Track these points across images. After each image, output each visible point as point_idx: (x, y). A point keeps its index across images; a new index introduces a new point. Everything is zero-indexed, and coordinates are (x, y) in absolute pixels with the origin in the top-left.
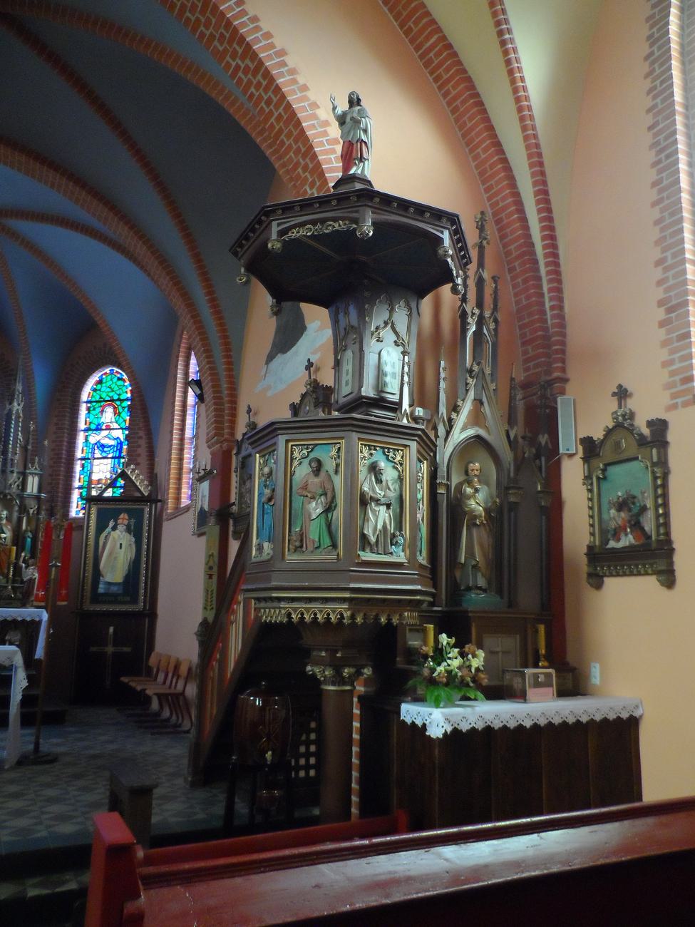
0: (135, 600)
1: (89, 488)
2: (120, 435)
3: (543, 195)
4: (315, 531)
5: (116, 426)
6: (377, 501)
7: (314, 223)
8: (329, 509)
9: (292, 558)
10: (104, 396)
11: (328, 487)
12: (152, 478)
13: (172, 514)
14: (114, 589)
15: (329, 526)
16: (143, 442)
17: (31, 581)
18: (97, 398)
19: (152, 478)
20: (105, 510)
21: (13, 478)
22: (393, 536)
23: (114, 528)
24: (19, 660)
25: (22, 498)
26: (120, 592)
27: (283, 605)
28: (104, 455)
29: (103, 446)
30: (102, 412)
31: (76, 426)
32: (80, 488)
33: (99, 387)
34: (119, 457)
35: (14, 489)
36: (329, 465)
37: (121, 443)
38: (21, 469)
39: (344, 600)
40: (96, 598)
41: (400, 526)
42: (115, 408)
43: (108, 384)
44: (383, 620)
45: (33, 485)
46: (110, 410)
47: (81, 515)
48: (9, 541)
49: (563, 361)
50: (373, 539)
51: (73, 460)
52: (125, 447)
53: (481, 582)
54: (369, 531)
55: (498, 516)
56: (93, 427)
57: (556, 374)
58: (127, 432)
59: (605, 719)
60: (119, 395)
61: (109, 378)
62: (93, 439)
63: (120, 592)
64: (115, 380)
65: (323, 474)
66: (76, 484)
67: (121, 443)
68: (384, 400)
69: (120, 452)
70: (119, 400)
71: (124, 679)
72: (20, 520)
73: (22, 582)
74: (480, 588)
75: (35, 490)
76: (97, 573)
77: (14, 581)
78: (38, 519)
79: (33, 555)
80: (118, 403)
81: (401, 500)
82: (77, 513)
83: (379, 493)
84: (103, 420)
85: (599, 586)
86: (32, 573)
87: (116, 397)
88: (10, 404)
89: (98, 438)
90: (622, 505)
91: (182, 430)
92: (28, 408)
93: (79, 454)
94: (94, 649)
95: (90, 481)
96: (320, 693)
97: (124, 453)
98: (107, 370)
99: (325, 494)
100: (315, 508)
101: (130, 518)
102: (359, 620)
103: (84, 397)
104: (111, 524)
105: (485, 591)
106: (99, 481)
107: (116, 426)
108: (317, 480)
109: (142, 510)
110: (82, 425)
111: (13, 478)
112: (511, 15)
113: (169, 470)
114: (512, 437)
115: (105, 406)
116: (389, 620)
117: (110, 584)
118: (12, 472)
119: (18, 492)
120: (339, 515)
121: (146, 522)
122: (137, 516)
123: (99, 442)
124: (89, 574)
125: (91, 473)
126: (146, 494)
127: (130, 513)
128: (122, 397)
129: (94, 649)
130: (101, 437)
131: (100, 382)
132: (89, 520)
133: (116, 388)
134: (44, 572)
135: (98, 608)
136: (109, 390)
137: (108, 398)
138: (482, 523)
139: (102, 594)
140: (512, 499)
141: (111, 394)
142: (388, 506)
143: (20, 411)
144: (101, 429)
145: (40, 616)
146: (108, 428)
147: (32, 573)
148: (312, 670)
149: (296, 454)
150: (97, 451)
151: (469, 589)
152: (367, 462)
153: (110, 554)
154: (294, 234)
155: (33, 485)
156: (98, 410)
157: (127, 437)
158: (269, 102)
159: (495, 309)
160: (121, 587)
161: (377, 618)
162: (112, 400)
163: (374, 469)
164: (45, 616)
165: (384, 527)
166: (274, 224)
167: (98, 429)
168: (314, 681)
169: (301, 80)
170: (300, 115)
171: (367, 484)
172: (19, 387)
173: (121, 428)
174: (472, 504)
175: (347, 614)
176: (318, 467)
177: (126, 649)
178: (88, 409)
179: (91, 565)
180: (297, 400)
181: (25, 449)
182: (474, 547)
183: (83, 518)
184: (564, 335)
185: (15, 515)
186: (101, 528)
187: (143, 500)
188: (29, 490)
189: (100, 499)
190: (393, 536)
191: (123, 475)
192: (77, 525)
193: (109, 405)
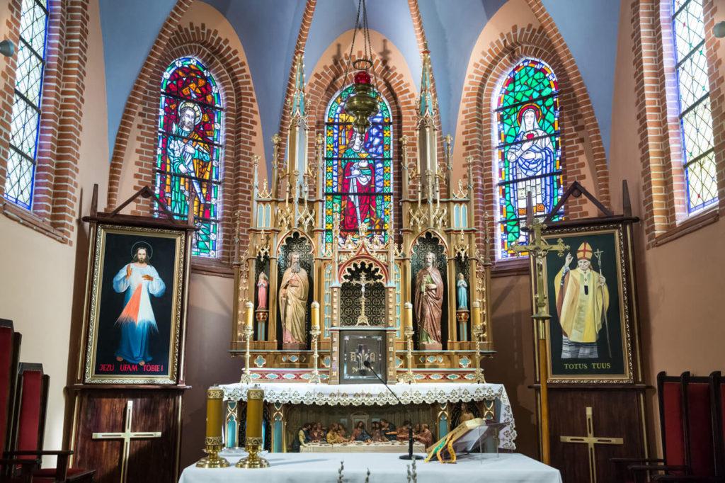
5: (541, 133)
10: (519, 97)
14: (584, 352)
23: (574, 265)
30: (520, 119)
33: (511, 87)
42: (536, 110)
43: (523, 81)
60: (540, 91)
70: (541, 98)
80: (540, 102)
87: (536, 95)
101: (594, 250)
110: (496, 141)
115: (523, 110)
117: (577, 345)
122: (604, 244)
127: (595, 242)
136: (525, 88)
137: (525, 99)
141: (528, 94)
146: (530, 137)
162: (532, 100)
173: (550, 135)
186: (555, 263)
193: (528, 108)
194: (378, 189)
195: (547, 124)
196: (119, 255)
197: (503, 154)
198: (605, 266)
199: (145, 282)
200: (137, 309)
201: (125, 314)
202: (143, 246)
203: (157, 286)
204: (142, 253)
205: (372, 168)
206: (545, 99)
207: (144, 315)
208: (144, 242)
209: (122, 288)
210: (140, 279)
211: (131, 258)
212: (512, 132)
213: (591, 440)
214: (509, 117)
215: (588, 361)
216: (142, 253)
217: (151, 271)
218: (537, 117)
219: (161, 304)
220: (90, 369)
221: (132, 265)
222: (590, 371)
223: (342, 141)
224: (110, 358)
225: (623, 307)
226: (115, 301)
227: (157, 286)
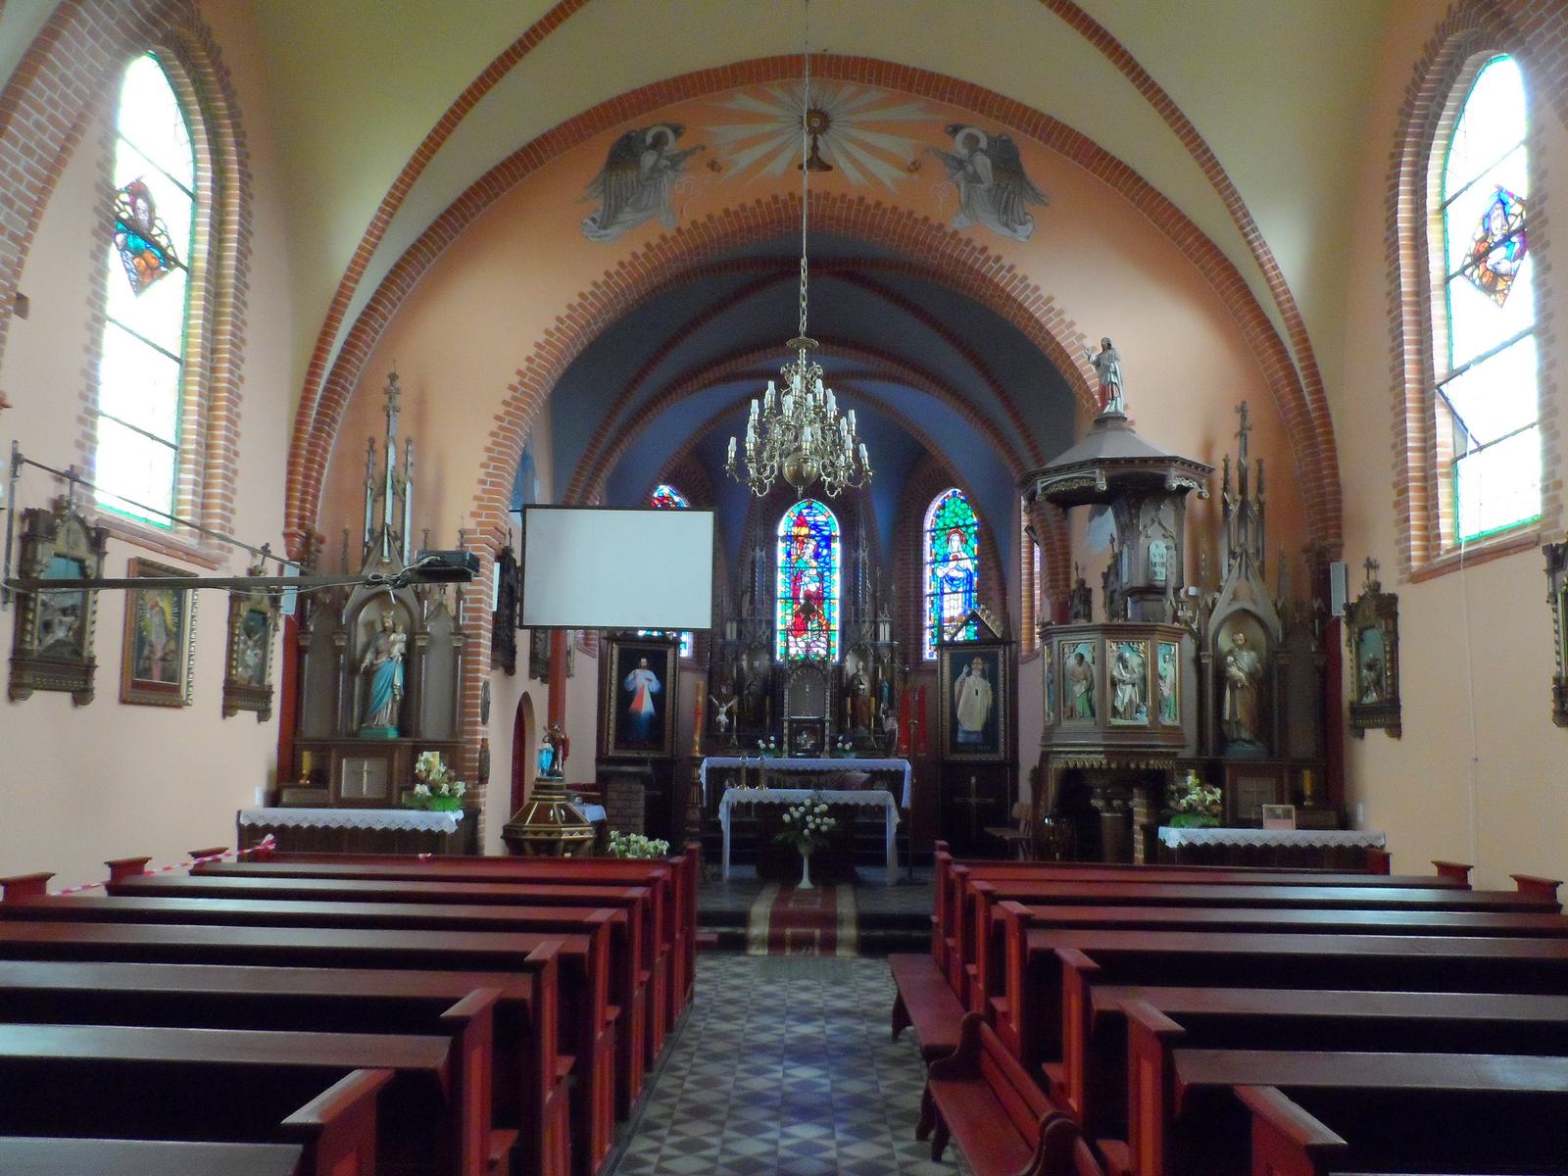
0: (995, 748)
1: (941, 631)
2: (969, 565)
3: (1312, 370)
4: (1081, 705)
5: (964, 555)
6: (1124, 682)
7: (1066, 480)
8: (1089, 689)
9: (1065, 724)
10: (948, 522)
11: (1089, 674)
12: (1006, 619)
13: (1027, 656)
14: (973, 738)
15: (1090, 701)
16: (993, 574)
17: (892, 732)
18: (941, 525)
19: (1006, 619)
20: (959, 655)
21: (866, 628)
22: (1139, 706)
23: (969, 674)
24: (891, 801)
25: (876, 648)
26: (980, 741)
27: (1063, 756)
28: (954, 589)
29: (952, 579)
30: (948, 541)
31: (922, 559)
32: (932, 627)
33: (942, 512)
34: (971, 591)
35: (868, 640)
36: (1088, 658)
37: (971, 575)
38: (872, 618)
39: (1101, 753)
40: (956, 747)
41: (1144, 698)
42: (961, 535)
43: (951, 508)
44: (1132, 766)
45: (885, 633)
46: (956, 538)
47: (935, 657)
48: (867, 692)
49: (1339, 527)
50: (1121, 710)
51: (922, 564)
52: (976, 579)
53: (1245, 735)
54: (1118, 704)
55: (1264, 681)
56: (939, 558)
57: (1332, 540)
58: (976, 562)
59: (1326, 846)
60: (964, 520)
61: (952, 500)
62: (940, 573)
63: (980, 741)
64: (959, 502)
65: (1084, 664)
66: (928, 623)
67: (971, 575)
68: (1155, 587)
69: (971, 585)
70: (965, 525)
71: (989, 830)
72: (876, 670)
73: (883, 732)
74: (1244, 740)
75: (887, 638)
76: (955, 722)
77: (875, 732)
78: (892, 668)
79: (891, 706)
80: (964, 529)
81: (1144, 679)
82: (931, 655)
83: (1126, 676)
84: (949, 550)
85: (1362, 736)
86: (891, 724)
87: (961, 523)
88: (856, 552)
89: (946, 570)
90: (1371, 667)
91: (1031, 563)
92: (873, 555)
93: (928, 590)
94: (957, 800)
95: (941, 620)
96: (1100, 818)
97: (975, 586)
98: (950, 492)
99: (1086, 679)
100: (1079, 689)
101: (983, 663)
102: (1114, 766)
103: (928, 525)
104: (965, 669)
105: (1248, 742)
106: (952, 619)
107: (964, 555)
108: (1080, 669)
109: (996, 655)
110: (928, 558)
111: (866, 628)
112: (1255, 215)
113: (1021, 608)
114: (1279, 605)
115: (950, 534)
116: (1138, 766)
117: (969, 733)
118: (864, 622)
119: (872, 642)
120: (1095, 693)
121: (1001, 666)
122: (991, 660)
123: (947, 575)
124: (947, 724)
125: (942, 609)
126: (999, 636)
127: (985, 657)
128: (968, 522)
129: (957, 800)
130: (950, 569)
131: (943, 507)
132: (942, 663)
133: (960, 512)
134: (903, 720)
135: (958, 757)
136: (953, 515)
137: (953, 525)
138: (1243, 686)
139: (963, 744)
140: (1282, 662)
141: (955, 520)
142: (1133, 685)
143: (866, 558)
144: (948, 561)
145: (904, 767)
146: (956, 559)
147: (891, 724)
148: (432, 640)
149: (1066, 650)
150: (946, 585)
151: (1234, 741)
152: (1116, 654)
153: (967, 700)
154: (1053, 490)
155: (885, 633)
156: (944, 538)
157: (977, 568)
158: (1044, 339)
159: (1260, 490)
160: (981, 736)
161: (1128, 765)
162: (958, 527)
163: (1121, 658)
164: (908, 767)
165: (1131, 701)
166: (1039, 482)
167: (946, 560)
168: (1096, 812)
169: (1068, 318)
170: (1068, 351)
171: (1117, 671)
172: (863, 533)
173: (970, 558)
174: (1234, 670)
175: (1104, 762)
176: (1081, 657)
177: (991, 800)
178: (933, 539)
179: (948, 711)
180: (1106, 570)
181: (874, 596)
182: (1236, 707)
183: (936, 662)
184: (1339, 501)
185: (871, 665)
186: (955, 674)
187: (995, 642)
188: (882, 638)
189: (952, 644)
190: (1139, 706)
191: (974, 617)
192: (932, 669)
193: (955, 532)
194: (825, 595)
195: (969, 548)
196: (628, 663)
197: (933, 570)
198: (991, 676)
199: (647, 683)
200: (641, 704)
201: (633, 706)
202: (644, 657)
203: (655, 685)
204: (644, 661)
205: (821, 576)
206: (968, 526)
207: (647, 706)
208: (806, 729)
209: (1513, 887)
210: (644, 680)
211: (637, 666)
212: (941, 552)
213: (973, 800)
214: (939, 538)
215: (976, 745)
216: (644, 661)
217: (651, 675)
218: (962, 541)
219: (658, 699)
220: (611, 746)
221: (637, 671)
222: (977, 752)
223: (793, 552)
224: (622, 740)
225: (1001, 706)
226: (626, 697)
227: (655, 685)
